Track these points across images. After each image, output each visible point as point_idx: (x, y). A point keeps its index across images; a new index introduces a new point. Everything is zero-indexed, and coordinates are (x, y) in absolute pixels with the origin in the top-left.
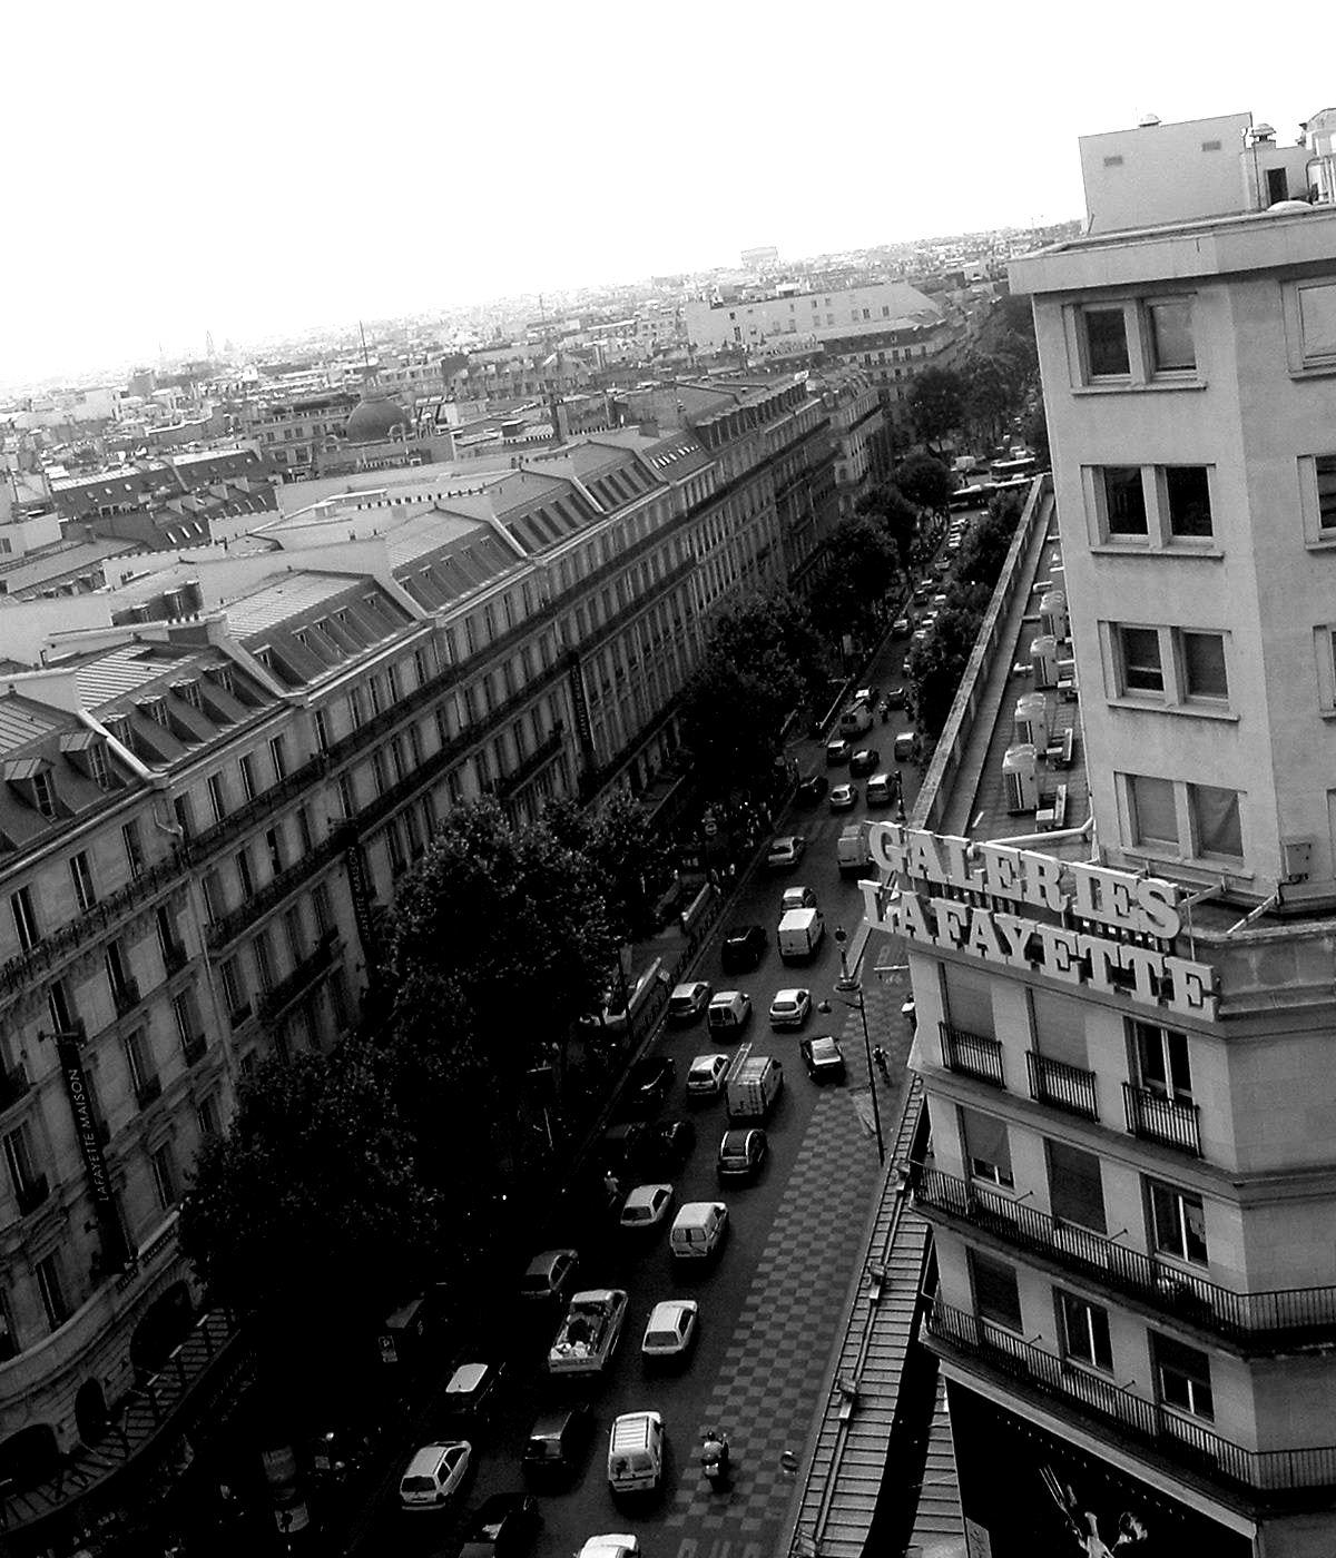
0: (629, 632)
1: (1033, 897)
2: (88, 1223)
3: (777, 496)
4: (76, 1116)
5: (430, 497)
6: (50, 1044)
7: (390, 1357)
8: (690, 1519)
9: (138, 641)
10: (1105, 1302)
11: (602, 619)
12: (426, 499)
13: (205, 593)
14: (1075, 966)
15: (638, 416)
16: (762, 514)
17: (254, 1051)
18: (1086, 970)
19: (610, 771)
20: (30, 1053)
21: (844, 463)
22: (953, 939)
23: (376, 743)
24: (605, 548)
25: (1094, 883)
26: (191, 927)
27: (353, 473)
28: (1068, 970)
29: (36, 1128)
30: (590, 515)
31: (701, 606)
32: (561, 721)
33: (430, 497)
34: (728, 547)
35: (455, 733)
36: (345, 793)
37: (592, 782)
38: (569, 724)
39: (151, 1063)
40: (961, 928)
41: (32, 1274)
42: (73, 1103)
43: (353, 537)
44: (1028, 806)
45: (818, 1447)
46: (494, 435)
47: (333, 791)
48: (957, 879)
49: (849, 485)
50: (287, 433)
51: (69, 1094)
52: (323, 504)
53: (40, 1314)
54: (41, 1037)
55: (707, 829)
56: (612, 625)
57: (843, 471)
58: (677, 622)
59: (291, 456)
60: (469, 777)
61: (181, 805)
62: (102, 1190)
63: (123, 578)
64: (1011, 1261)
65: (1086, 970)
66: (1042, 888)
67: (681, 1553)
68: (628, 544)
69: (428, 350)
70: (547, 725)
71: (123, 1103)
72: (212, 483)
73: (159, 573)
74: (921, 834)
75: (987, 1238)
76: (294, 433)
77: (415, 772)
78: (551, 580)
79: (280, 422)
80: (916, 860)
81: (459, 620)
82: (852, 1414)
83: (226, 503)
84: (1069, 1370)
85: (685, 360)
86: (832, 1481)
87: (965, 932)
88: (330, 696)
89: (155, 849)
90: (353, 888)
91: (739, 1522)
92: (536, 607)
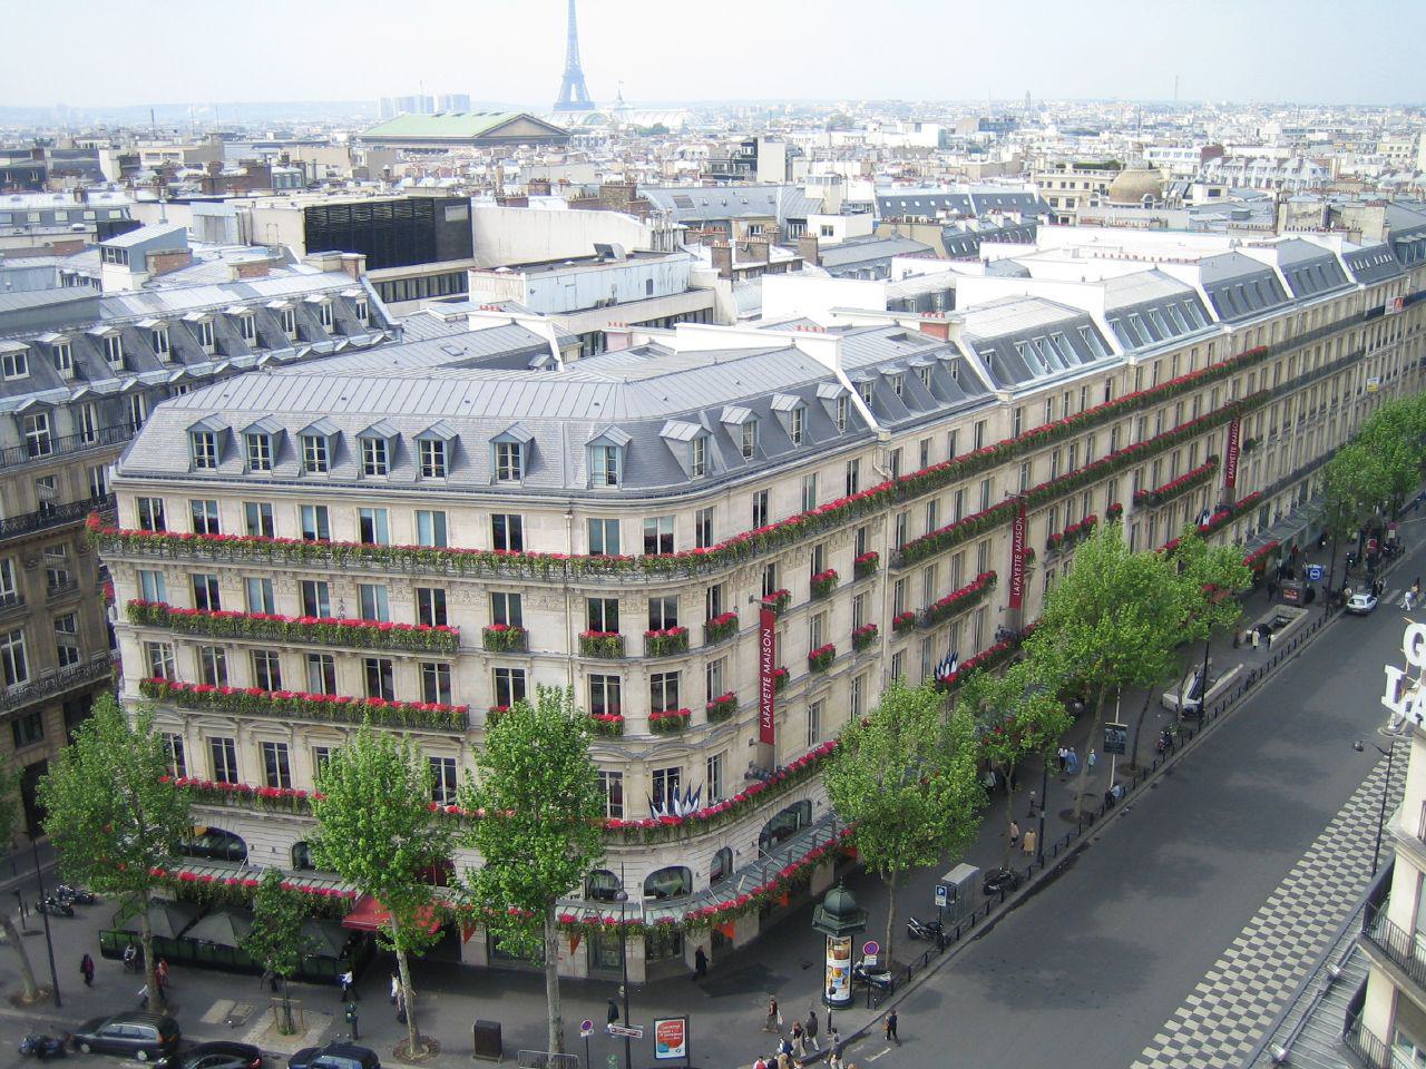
2: (752, 740)
4: (762, 662)
6: (756, 607)
7: (941, 901)
13: (961, 302)
15: (1347, 225)
16: (1417, 335)
17: (905, 650)
19: (1251, 503)
24: (1289, 328)
26: (883, 543)
29: (731, 663)
33: (1153, 259)
34: (1397, 347)
36: (1024, 476)
42: (762, 652)
43: (1084, 279)
51: (762, 646)
54: (751, 600)
56: (1278, 391)
58: (1335, 401)
61: (896, 458)
62: (767, 720)
63: (905, 273)
68: (1308, 329)
69: (1197, 136)
71: (799, 662)
72: (993, 213)
73: (934, 273)
77: (1191, 424)
79: (1059, 175)
85: (1407, 184)
88: (1031, 399)
90: (1014, 548)
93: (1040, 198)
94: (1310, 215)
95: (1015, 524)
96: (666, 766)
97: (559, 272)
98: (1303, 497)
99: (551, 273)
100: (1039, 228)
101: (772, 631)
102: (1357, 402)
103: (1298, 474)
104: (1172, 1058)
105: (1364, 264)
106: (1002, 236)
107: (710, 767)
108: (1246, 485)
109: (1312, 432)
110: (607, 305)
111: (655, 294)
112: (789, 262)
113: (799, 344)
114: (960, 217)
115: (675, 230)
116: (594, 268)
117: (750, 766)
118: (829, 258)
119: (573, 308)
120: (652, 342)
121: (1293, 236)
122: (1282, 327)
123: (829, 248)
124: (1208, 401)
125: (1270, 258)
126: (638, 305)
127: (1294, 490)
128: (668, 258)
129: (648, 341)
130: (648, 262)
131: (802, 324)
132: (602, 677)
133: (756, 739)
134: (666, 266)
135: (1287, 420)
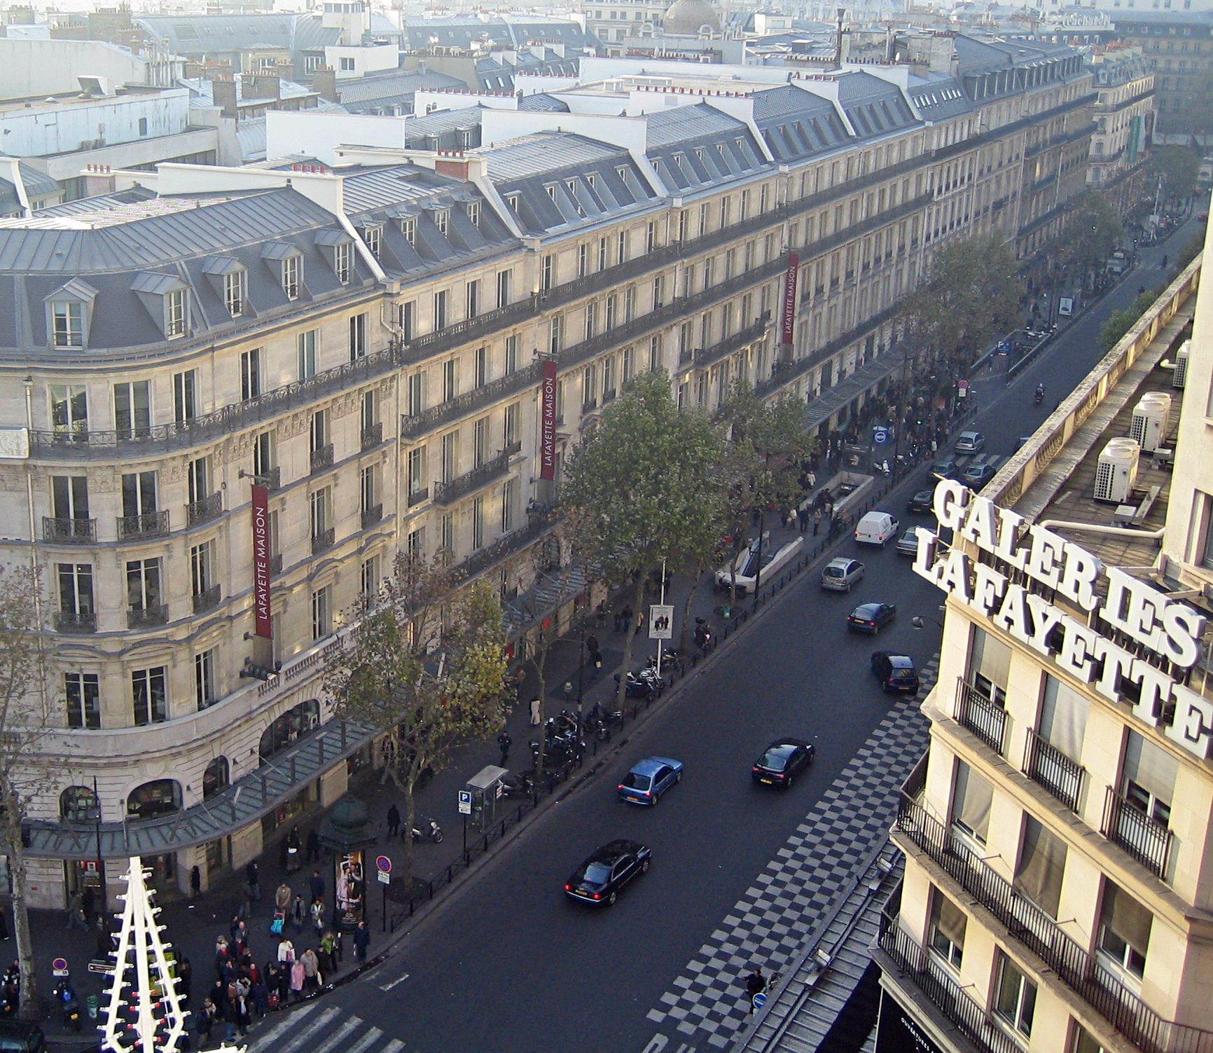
0: (853, 248)
1: (1066, 589)
3: (1027, 154)
4: (256, 546)
5: (700, 92)
6: (248, 482)
7: (465, 808)
8: (668, 1018)
9: (411, 164)
10: (1036, 977)
11: (830, 230)
12: (696, 92)
14: (1088, 665)
18: (1097, 673)
20: (229, 486)
21: (1102, 137)
22: (986, 606)
23: (593, 295)
24: (849, 169)
25: (1126, 593)
26: (391, 416)
27: (651, 58)
28: (1081, 666)
29: (221, 546)
30: (844, 139)
31: (928, 239)
32: (769, 312)
33: (700, 92)
35: (668, 300)
37: (785, 371)
38: (776, 316)
39: (331, 517)
40: (995, 597)
41: (191, 662)
44: (1116, 497)
45: (777, 1002)
46: (785, 49)
47: (545, 327)
48: (1003, 552)
49: (1102, 159)
50: (614, 14)
52: (614, 80)
53: (192, 693)
54: (241, 475)
55: (877, 437)
57: (1100, 145)
59: (612, 35)
60: (672, 342)
61: (407, 312)
62: (263, 610)
63: (428, 109)
64: (964, 910)
65: (1097, 673)
66: (1077, 584)
67: (651, 1045)
68: (871, 169)
70: (756, 313)
72: (534, 44)
74: (982, 503)
75: (950, 881)
76: (618, 15)
78: (789, 186)
80: (971, 524)
81: (696, 205)
82: (817, 983)
83: (541, 64)
84: (990, 1024)
85: (981, 16)
86: (779, 1035)
87: (998, 602)
89: (376, 340)
91: (709, 1034)
92: (771, 207)
93: (586, 28)
94: (875, 47)
95: (544, 386)
96: (147, 666)
97: (37, 108)
98: (869, 353)
99: (27, 111)
100: (582, 60)
101: (266, 508)
102: (925, 249)
103: (862, 329)
104: (724, 1016)
105: (931, 100)
106: (541, 68)
107: (198, 666)
108: (806, 337)
109: (878, 282)
110: (95, 148)
111: (150, 134)
112: (302, 98)
113: (296, 186)
114: (496, 49)
115: (172, 63)
116: (77, 106)
117: (246, 663)
118: (348, 95)
119: (54, 151)
120: (138, 186)
121: (855, 68)
122: (842, 167)
123: (350, 83)
124: (760, 250)
125: (829, 91)
126: (130, 146)
127: (859, 346)
128: (164, 94)
129: (132, 185)
130: (140, 98)
131: (314, 165)
132: (71, 566)
133: (252, 632)
134: (162, 103)
135: (834, 277)
